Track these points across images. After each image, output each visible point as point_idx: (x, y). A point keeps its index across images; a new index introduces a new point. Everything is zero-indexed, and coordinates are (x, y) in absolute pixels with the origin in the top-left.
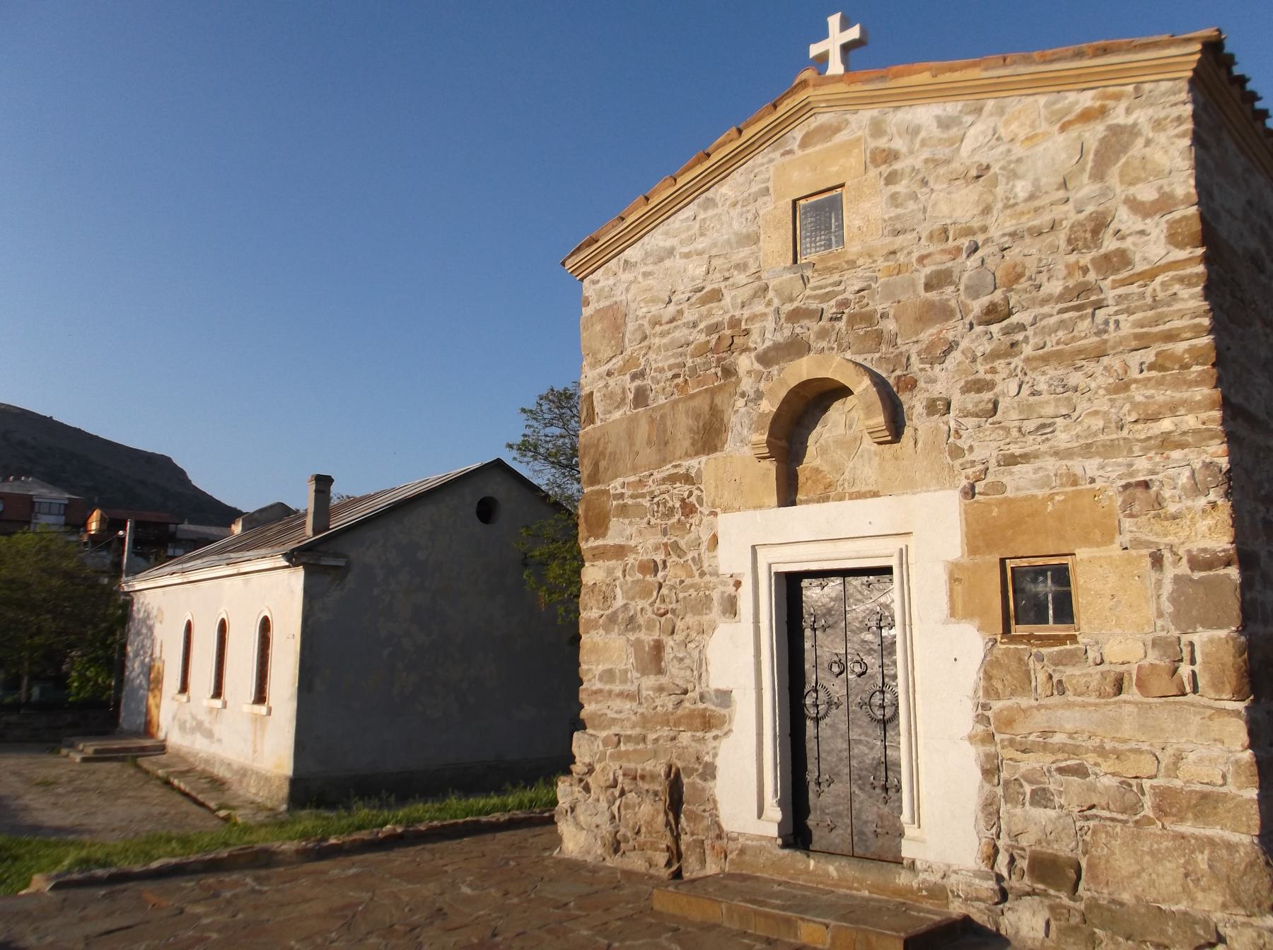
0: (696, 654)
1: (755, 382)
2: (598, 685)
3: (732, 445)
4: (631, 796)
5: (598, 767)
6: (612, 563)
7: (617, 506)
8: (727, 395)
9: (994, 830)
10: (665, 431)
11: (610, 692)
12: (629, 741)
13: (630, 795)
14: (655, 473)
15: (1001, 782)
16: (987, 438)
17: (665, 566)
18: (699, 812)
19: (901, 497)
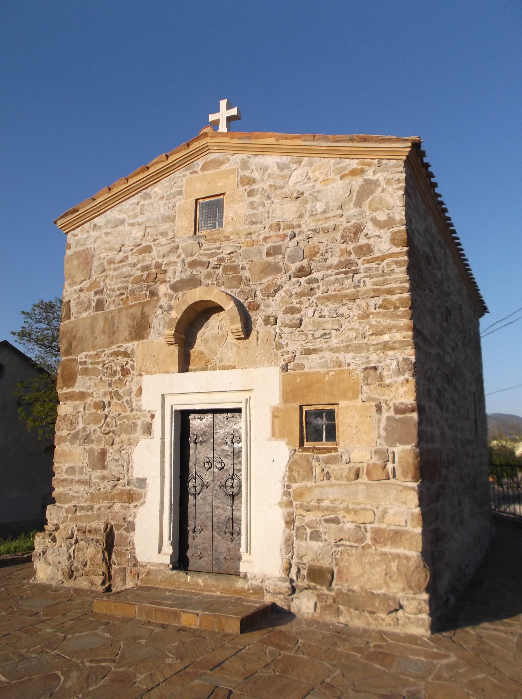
0: (126, 457)
2: (65, 476)
3: (153, 336)
4: (82, 543)
5: (62, 526)
6: (77, 403)
7: (82, 369)
8: (152, 307)
9: (290, 555)
10: (113, 326)
11: (72, 480)
12: (82, 510)
13: (81, 543)
14: (106, 350)
15: (295, 528)
16: (296, 339)
18: (123, 551)
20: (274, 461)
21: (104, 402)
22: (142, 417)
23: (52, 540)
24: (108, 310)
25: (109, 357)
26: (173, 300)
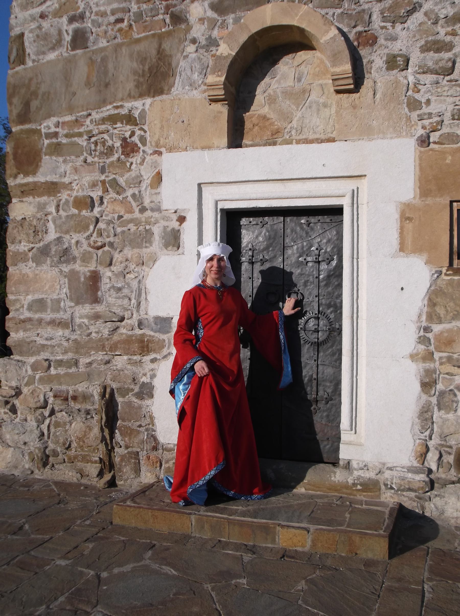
0: (135, 284)
1: (209, 29)
2: (27, 314)
3: (180, 89)
4: (62, 416)
5: (25, 390)
6: (44, 199)
7: (49, 145)
8: (177, 40)
9: (427, 433)
10: (106, 73)
11: (40, 321)
12: (60, 365)
13: (59, 415)
14: (94, 113)
15: (437, 393)
16: (445, 94)
17: (102, 203)
18: (135, 427)
19: (356, 143)
20: (402, 289)
21: (92, 198)
22: (162, 221)
23: (10, 410)
24: (95, 48)
25: (99, 124)
26: (217, 28)
